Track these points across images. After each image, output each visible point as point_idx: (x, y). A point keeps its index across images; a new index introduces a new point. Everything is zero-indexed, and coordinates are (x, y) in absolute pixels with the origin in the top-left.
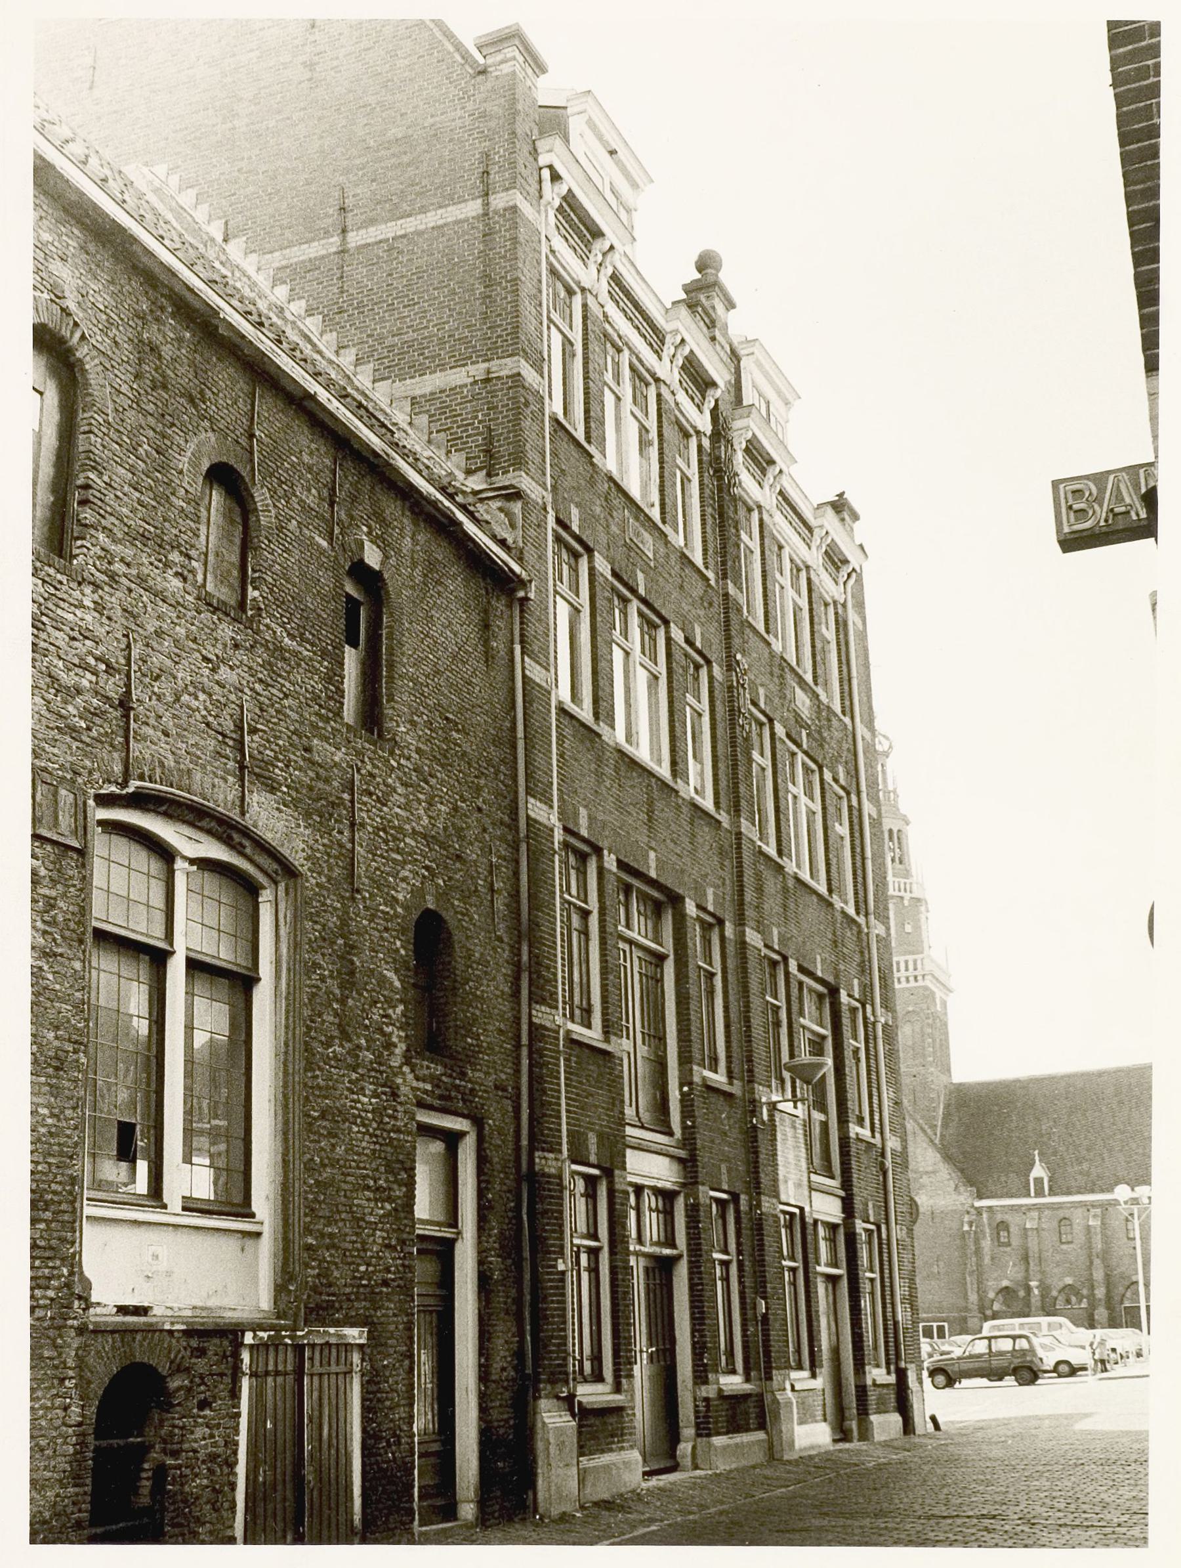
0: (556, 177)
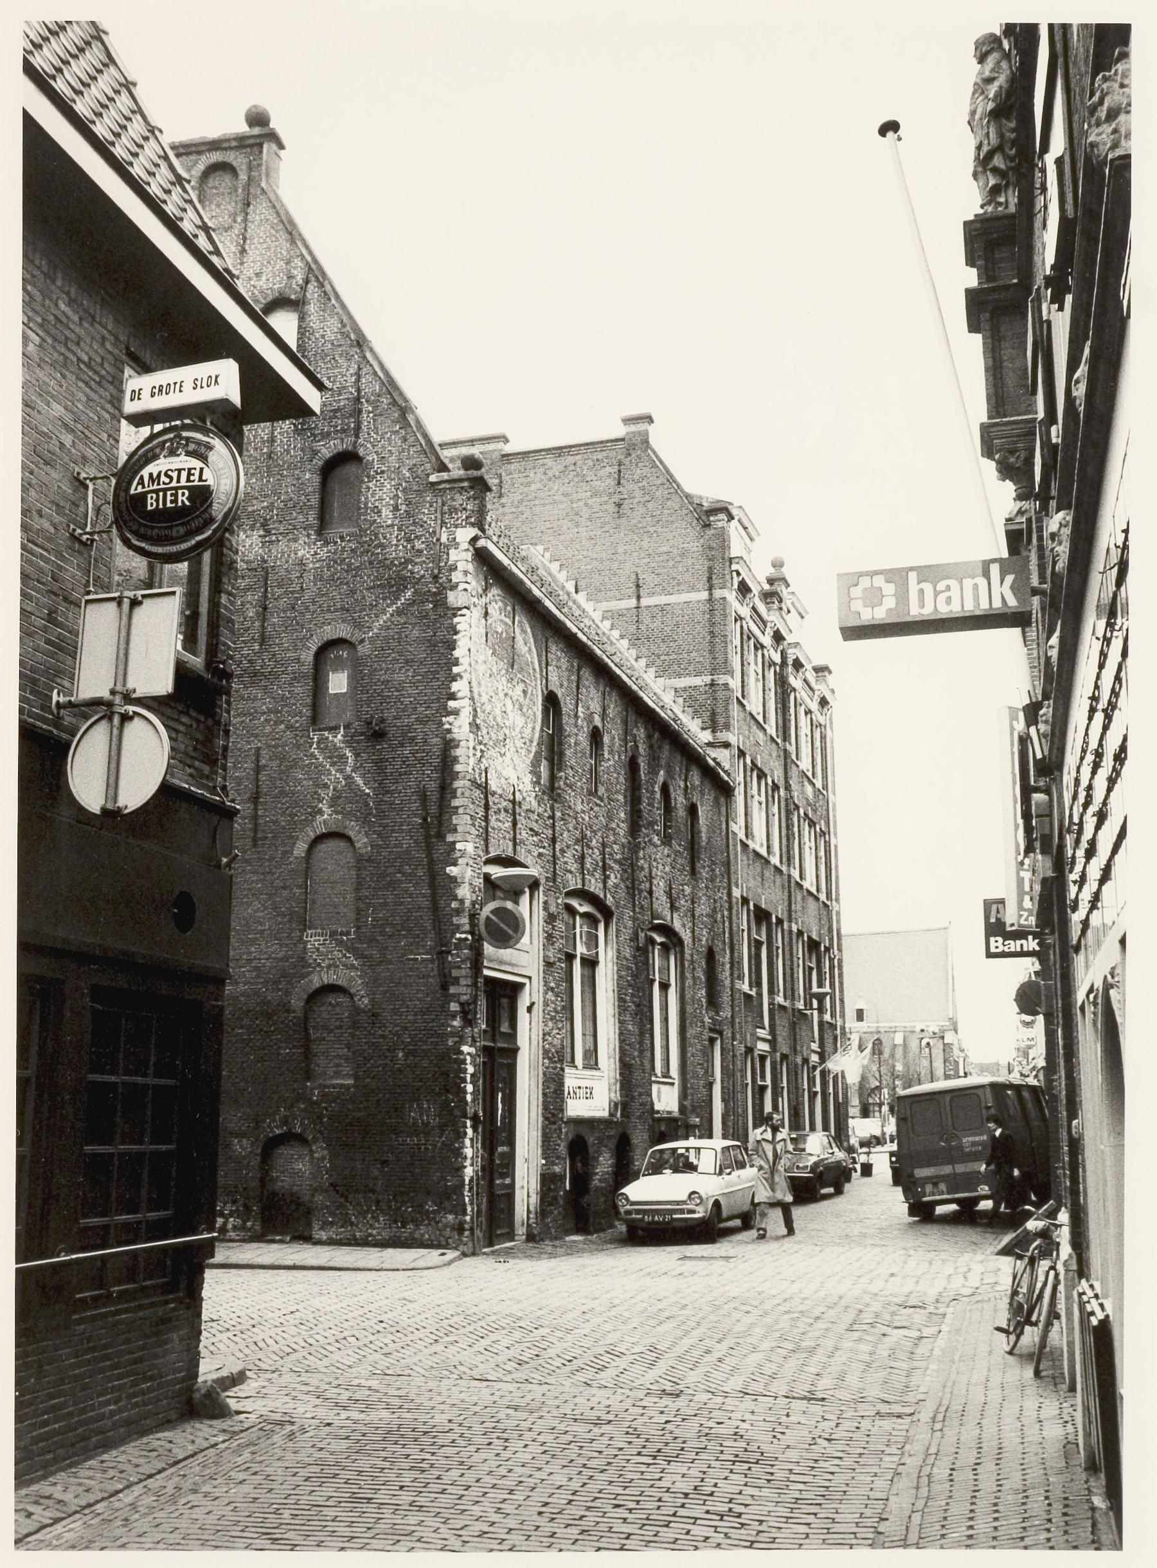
0: (738, 574)
